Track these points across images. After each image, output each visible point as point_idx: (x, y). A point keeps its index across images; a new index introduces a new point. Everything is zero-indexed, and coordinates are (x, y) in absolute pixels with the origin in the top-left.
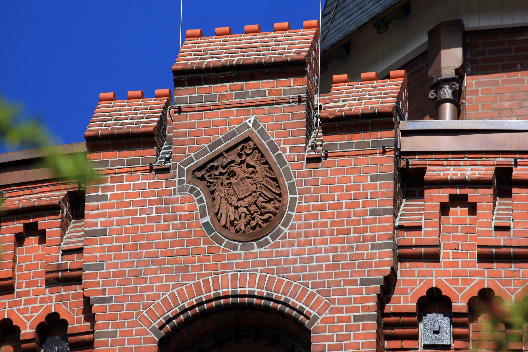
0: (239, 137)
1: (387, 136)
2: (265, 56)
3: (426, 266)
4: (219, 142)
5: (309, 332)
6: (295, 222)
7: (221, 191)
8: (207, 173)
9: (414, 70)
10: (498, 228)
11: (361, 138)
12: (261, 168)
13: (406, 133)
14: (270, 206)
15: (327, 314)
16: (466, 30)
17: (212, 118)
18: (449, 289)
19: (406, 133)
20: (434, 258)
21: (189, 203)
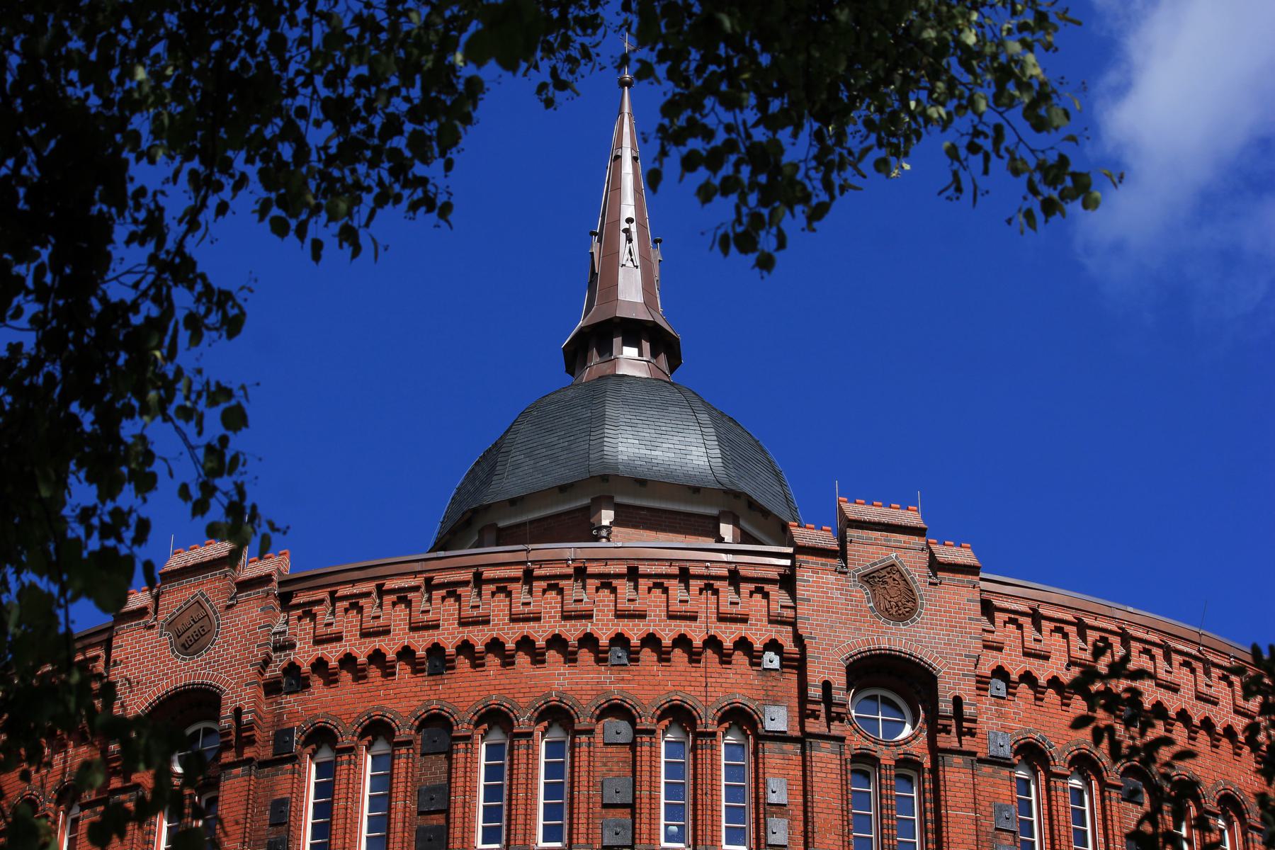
0: (887, 563)
1: (976, 579)
2: (885, 520)
3: (995, 653)
4: (875, 564)
5: (935, 678)
6: (925, 614)
7: (879, 591)
8: (868, 579)
9: (638, 502)
10: (576, 601)
11: (960, 577)
12: (902, 583)
13: (982, 579)
14: (910, 604)
15: (946, 669)
16: (119, 422)
17: (872, 549)
18: (1008, 668)
19: (982, 579)
20: (1000, 649)
21: (861, 593)
